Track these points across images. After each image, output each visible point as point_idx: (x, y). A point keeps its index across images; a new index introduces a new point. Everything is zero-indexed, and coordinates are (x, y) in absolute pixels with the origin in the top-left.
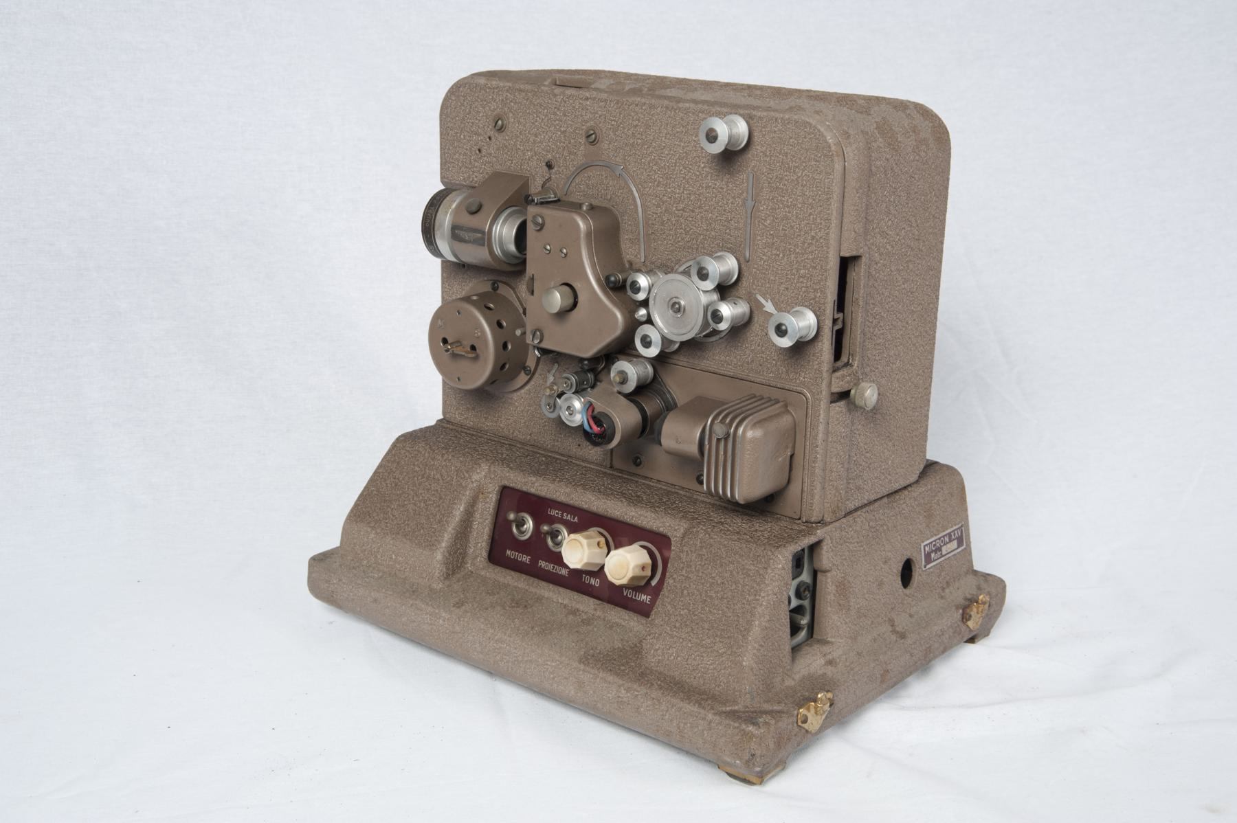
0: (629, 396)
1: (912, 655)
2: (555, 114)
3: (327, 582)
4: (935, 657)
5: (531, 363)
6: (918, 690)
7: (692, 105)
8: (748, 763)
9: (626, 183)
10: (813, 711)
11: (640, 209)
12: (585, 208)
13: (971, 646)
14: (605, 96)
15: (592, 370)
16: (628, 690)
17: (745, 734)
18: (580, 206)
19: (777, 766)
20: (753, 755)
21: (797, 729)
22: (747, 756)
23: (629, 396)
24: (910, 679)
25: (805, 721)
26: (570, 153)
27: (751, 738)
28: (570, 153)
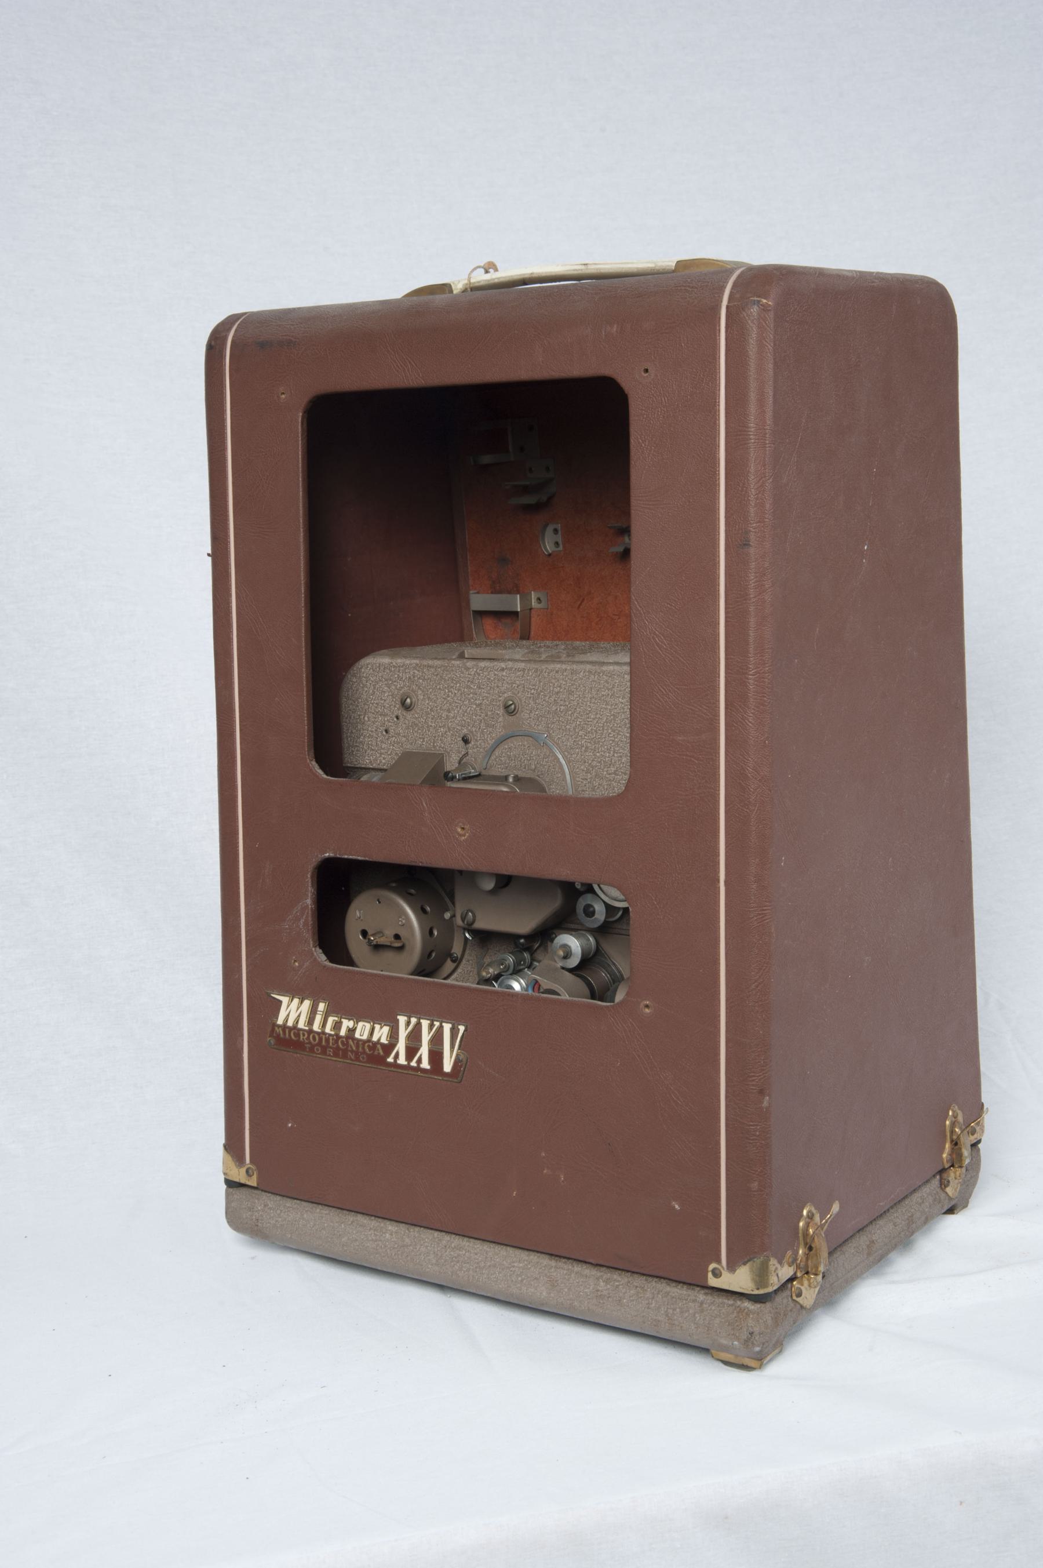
0: (571, 971)
1: (895, 1225)
2: (469, 687)
3: (250, 1209)
4: (918, 1228)
5: (457, 950)
6: (903, 1265)
7: (616, 668)
8: (747, 1342)
9: (551, 751)
10: (806, 1282)
11: (568, 777)
12: (511, 780)
13: (951, 1218)
14: (522, 665)
15: (528, 949)
16: (607, 1281)
17: (741, 1311)
18: (506, 778)
19: (775, 1347)
20: (751, 1334)
21: (792, 1305)
22: (744, 1335)
23: (571, 971)
24: (892, 1255)
25: (799, 1295)
26: (488, 726)
27: (748, 1315)
28: (488, 726)
